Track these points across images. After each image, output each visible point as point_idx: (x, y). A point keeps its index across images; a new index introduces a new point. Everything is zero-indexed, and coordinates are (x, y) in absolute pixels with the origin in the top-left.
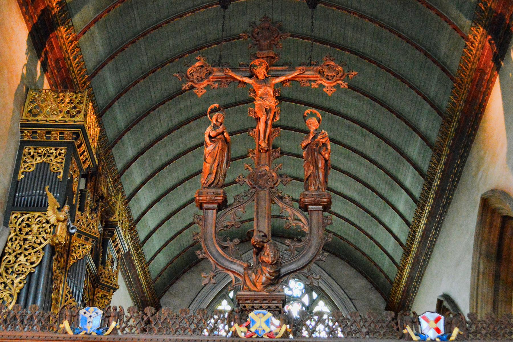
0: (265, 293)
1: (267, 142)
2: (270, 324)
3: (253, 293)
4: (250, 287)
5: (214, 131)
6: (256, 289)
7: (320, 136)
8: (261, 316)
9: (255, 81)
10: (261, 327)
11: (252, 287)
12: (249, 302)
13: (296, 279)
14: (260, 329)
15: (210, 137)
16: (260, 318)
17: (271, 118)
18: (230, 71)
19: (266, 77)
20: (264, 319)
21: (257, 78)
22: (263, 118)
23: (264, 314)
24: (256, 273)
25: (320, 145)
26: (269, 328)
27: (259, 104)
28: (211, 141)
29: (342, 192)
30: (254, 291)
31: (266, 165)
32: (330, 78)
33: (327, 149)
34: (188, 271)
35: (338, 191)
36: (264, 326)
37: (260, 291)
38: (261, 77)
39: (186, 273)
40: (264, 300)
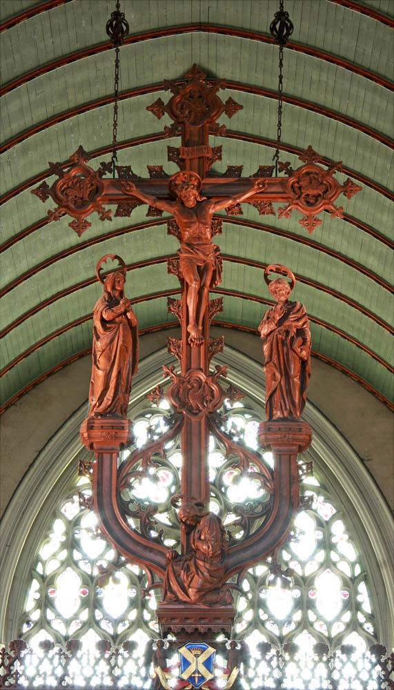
0: (202, 607)
1: (201, 328)
2: (212, 668)
3: (183, 607)
4: (180, 597)
5: (109, 311)
6: (185, 598)
7: (292, 317)
8: (199, 652)
9: (178, 210)
10: (199, 673)
11: (181, 596)
12: (177, 621)
13: (247, 416)
14: (197, 675)
15: (103, 321)
16: (195, 655)
17: (208, 283)
18: (134, 189)
19: (198, 202)
20: (202, 658)
21: (182, 203)
22: (194, 286)
23: (203, 650)
24: (188, 570)
25: (293, 334)
26: (211, 672)
27: (187, 258)
28: (105, 329)
29: (343, 252)
30: (185, 603)
31: (201, 370)
32: (312, 201)
33: (304, 340)
34: (18, 403)
35: (337, 249)
36: (202, 669)
37: (195, 604)
38: (191, 203)
39: (12, 408)
40: (201, 619)
